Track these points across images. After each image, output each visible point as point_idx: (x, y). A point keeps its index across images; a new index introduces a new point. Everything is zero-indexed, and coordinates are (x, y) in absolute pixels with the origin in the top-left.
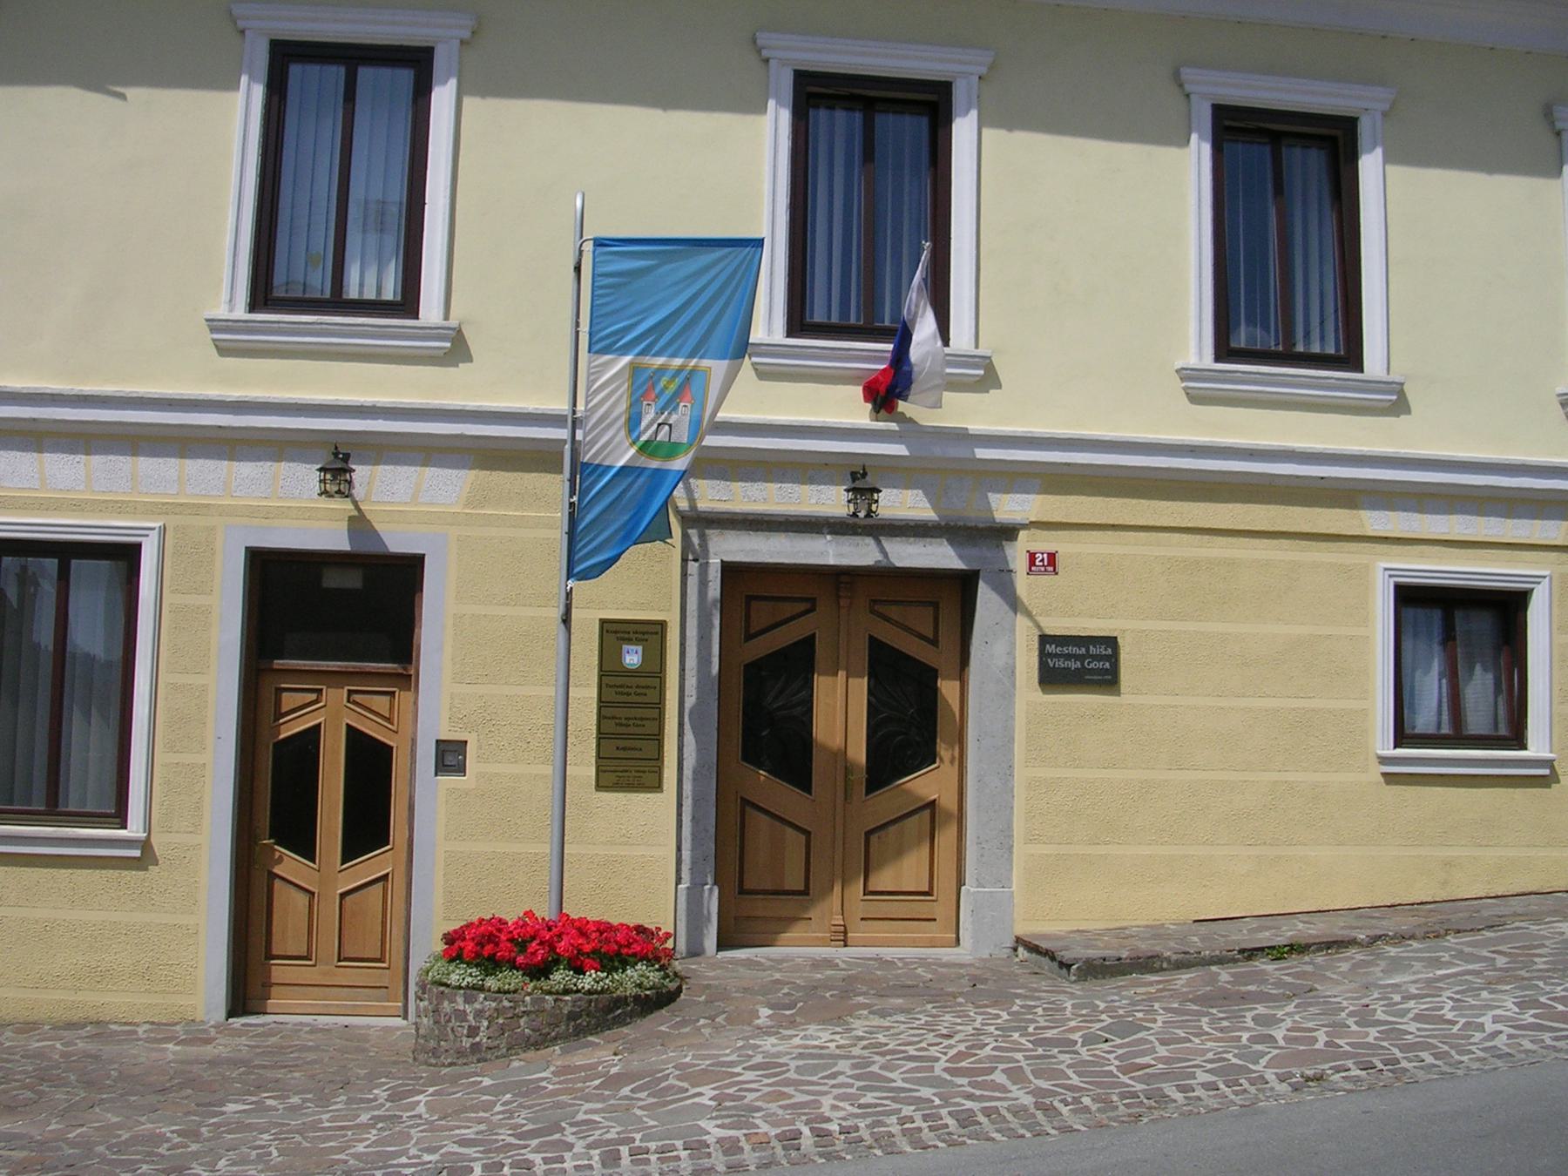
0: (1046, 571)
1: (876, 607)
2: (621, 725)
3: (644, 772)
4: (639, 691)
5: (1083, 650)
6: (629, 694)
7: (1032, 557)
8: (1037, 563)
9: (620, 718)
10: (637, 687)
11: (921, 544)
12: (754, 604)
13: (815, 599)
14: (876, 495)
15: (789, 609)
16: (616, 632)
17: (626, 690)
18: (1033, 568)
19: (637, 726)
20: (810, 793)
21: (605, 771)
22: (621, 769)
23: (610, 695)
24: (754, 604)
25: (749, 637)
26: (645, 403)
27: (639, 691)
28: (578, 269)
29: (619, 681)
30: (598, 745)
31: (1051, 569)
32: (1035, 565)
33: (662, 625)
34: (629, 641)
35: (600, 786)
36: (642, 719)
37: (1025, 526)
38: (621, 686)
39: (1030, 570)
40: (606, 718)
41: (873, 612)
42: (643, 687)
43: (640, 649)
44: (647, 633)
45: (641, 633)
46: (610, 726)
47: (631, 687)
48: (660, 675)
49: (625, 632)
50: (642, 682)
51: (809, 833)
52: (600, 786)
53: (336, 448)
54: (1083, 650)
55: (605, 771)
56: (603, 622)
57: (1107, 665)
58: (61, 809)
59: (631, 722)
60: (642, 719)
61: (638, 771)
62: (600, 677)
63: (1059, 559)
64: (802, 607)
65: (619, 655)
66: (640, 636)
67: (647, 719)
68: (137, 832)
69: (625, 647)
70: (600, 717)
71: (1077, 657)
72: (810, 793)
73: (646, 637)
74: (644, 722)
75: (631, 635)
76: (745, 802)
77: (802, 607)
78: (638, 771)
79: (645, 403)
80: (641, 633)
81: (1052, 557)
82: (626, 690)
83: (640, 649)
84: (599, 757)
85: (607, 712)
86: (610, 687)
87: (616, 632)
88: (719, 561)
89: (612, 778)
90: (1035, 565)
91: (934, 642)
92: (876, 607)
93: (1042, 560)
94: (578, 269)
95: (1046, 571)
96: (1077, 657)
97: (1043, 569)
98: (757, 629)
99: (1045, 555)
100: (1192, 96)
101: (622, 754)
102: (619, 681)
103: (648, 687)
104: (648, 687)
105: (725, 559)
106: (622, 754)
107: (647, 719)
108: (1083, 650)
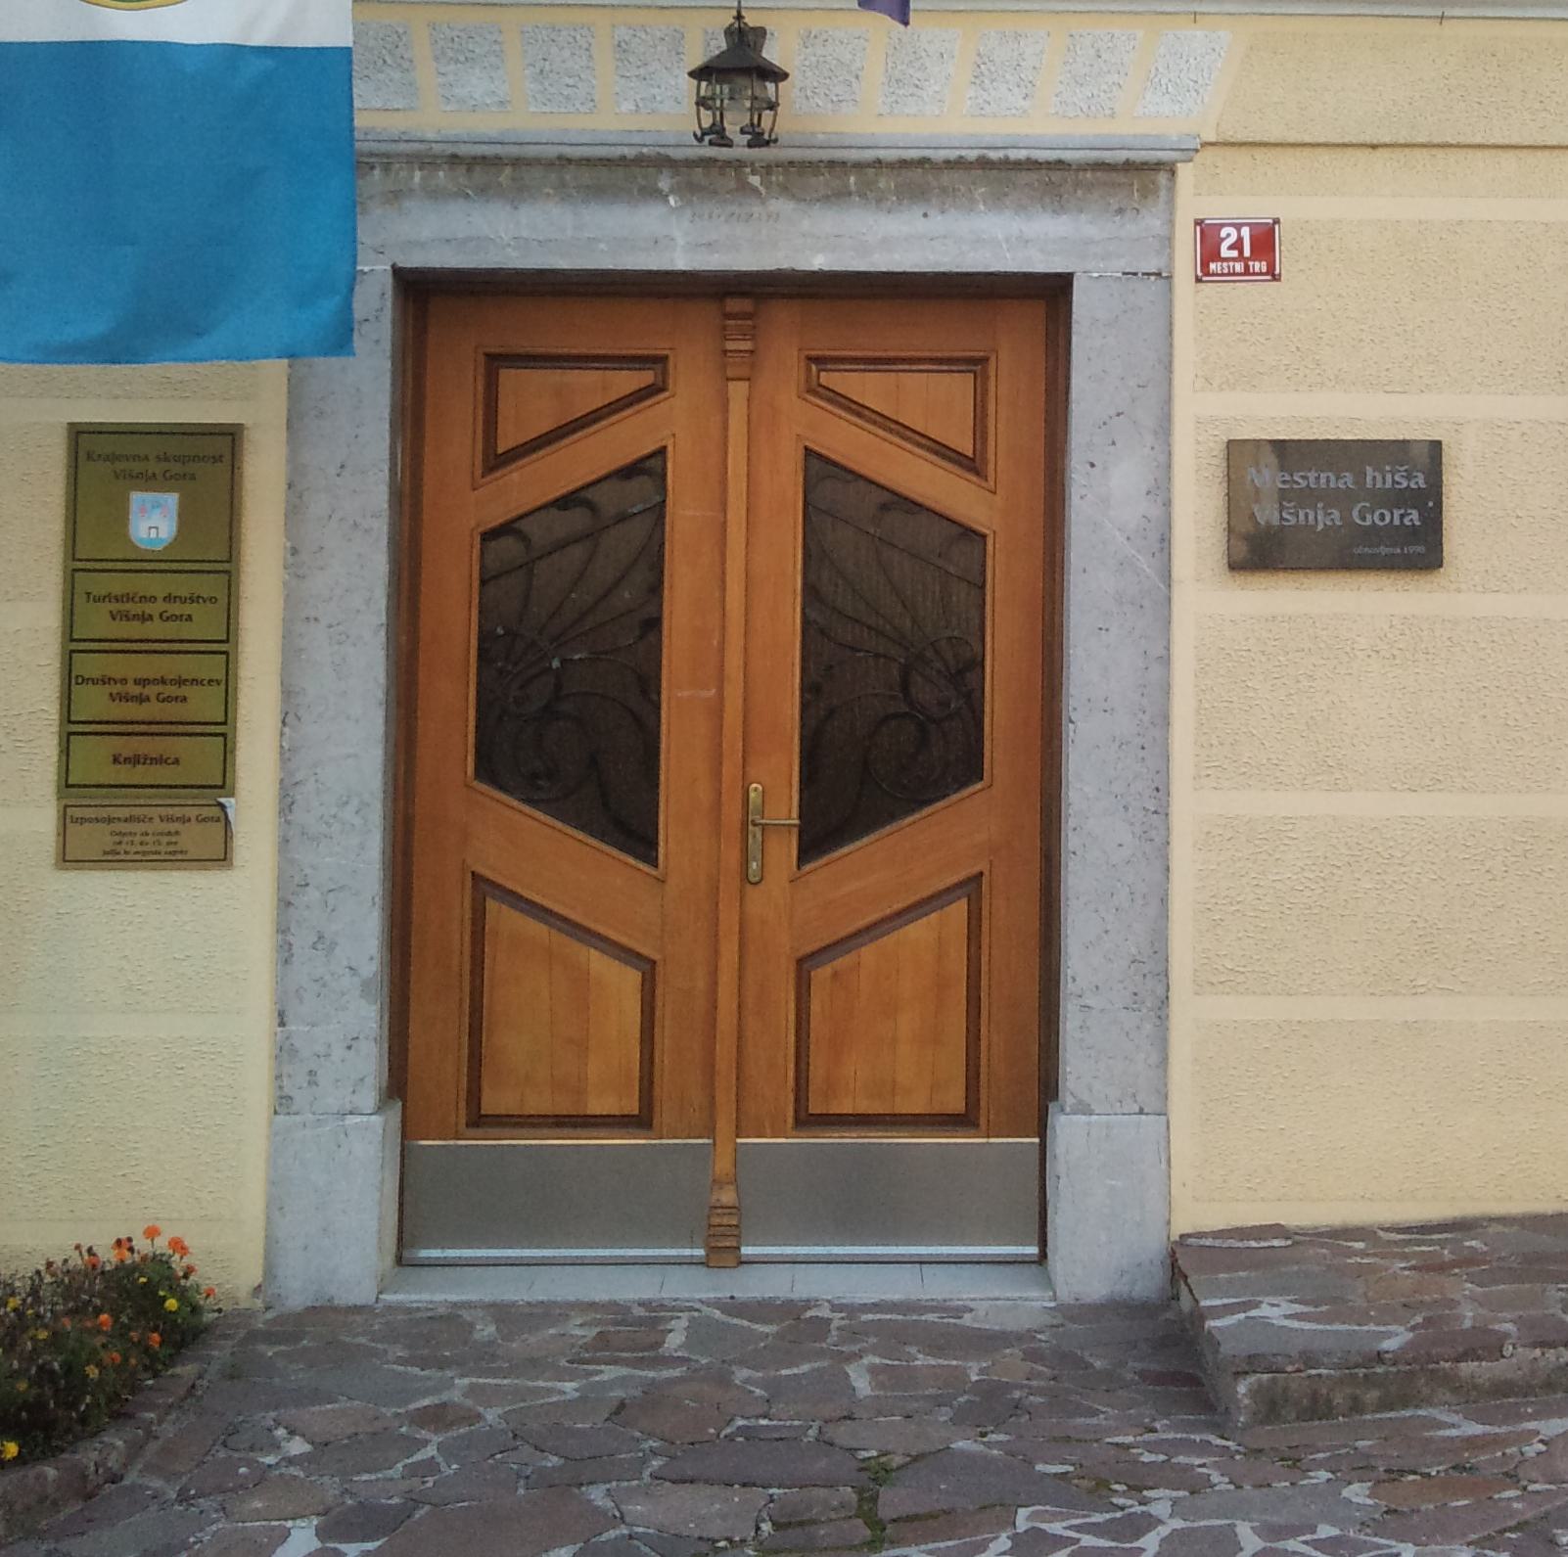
0: (1247, 272)
1: (825, 378)
3: (185, 820)
4: (176, 609)
6: (145, 618)
7: (1208, 237)
8: (1225, 253)
9: (124, 681)
10: (168, 598)
12: (508, 377)
14: (770, 86)
15: (591, 387)
16: (113, 458)
18: (1213, 266)
19: (168, 699)
20: (654, 863)
21: (82, 820)
22: (124, 812)
23: (98, 623)
24: (508, 377)
25: (496, 461)
27: (176, 609)
29: (116, 584)
30: (65, 751)
31: (1259, 266)
33: (231, 436)
34: (149, 481)
35: (67, 859)
37: (1189, 153)
38: (128, 598)
39: (1205, 265)
40: (86, 681)
41: (816, 390)
43: (172, 500)
44: (195, 458)
45: (177, 459)
46: (94, 703)
48: (226, 568)
49: (136, 458)
50: (183, 585)
51: (800, 962)
53: (739, 17)
54: (1349, 478)
55: (82, 820)
56: (79, 435)
59: (151, 691)
61: (170, 819)
62: (71, 576)
63: (1283, 237)
64: (628, 381)
66: (176, 468)
67: (195, 681)
68: (790, 818)
70: (71, 680)
72: (654, 863)
74: (185, 691)
75: (154, 467)
76: (482, 886)
77: (628, 381)
78: (170, 819)
80: (177, 459)
81: (1264, 241)
83: (172, 500)
85: (90, 665)
86: (98, 600)
87: (113, 458)
88: (389, 268)
89: (98, 837)
91: (972, 465)
92: (825, 378)
93: (1238, 245)
95: (1247, 272)
97: (1239, 267)
99: (1246, 232)
102: (116, 584)
103: (194, 599)
104: (194, 599)
107: (195, 681)
108: (1349, 478)
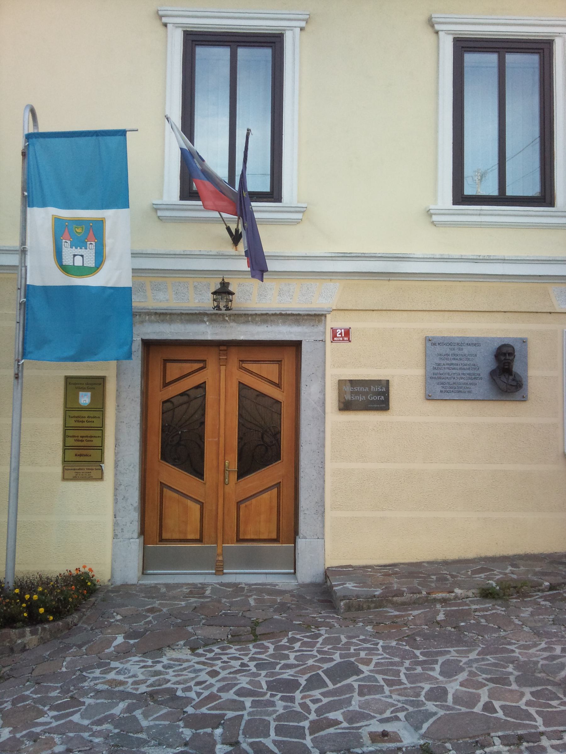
0: (343, 340)
1: (243, 365)
2: (78, 441)
5: (367, 388)
6: (83, 422)
7: (334, 332)
8: (338, 335)
9: (78, 437)
10: (88, 417)
11: (265, 326)
13: (205, 361)
14: (231, 296)
16: (75, 384)
17: (81, 419)
24: (169, 365)
25: (166, 385)
26: (89, 243)
28: (460, 281)
30: (64, 453)
31: (346, 339)
32: (336, 336)
33: (103, 379)
34: (84, 389)
35: (64, 479)
36: (91, 437)
37: (329, 312)
38: (79, 417)
41: (241, 368)
42: (92, 418)
45: (90, 384)
47: (85, 417)
48: (102, 410)
49: (81, 384)
50: (92, 414)
52: (64, 479)
55: (68, 469)
56: (67, 378)
57: (383, 398)
58: (512, 352)
59: (84, 439)
60: (91, 437)
61: (89, 469)
62: (65, 412)
64: (197, 366)
65: (77, 398)
66: (90, 386)
67: (95, 437)
69: (81, 393)
70: (65, 436)
71: (363, 393)
73: (94, 386)
74: (92, 439)
76: (163, 485)
78: (89, 469)
79: (89, 243)
80: (90, 384)
81: (347, 333)
82: (81, 419)
84: (64, 461)
86: (72, 417)
90: (336, 336)
92: (243, 365)
93: (341, 334)
94: (460, 281)
95: (343, 340)
96: (363, 393)
97: (341, 339)
98: (169, 381)
99: (343, 331)
100: (440, 33)
101: (78, 459)
103: (94, 417)
104: (94, 417)
105: (144, 338)
106: (78, 459)
107: (95, 437)
